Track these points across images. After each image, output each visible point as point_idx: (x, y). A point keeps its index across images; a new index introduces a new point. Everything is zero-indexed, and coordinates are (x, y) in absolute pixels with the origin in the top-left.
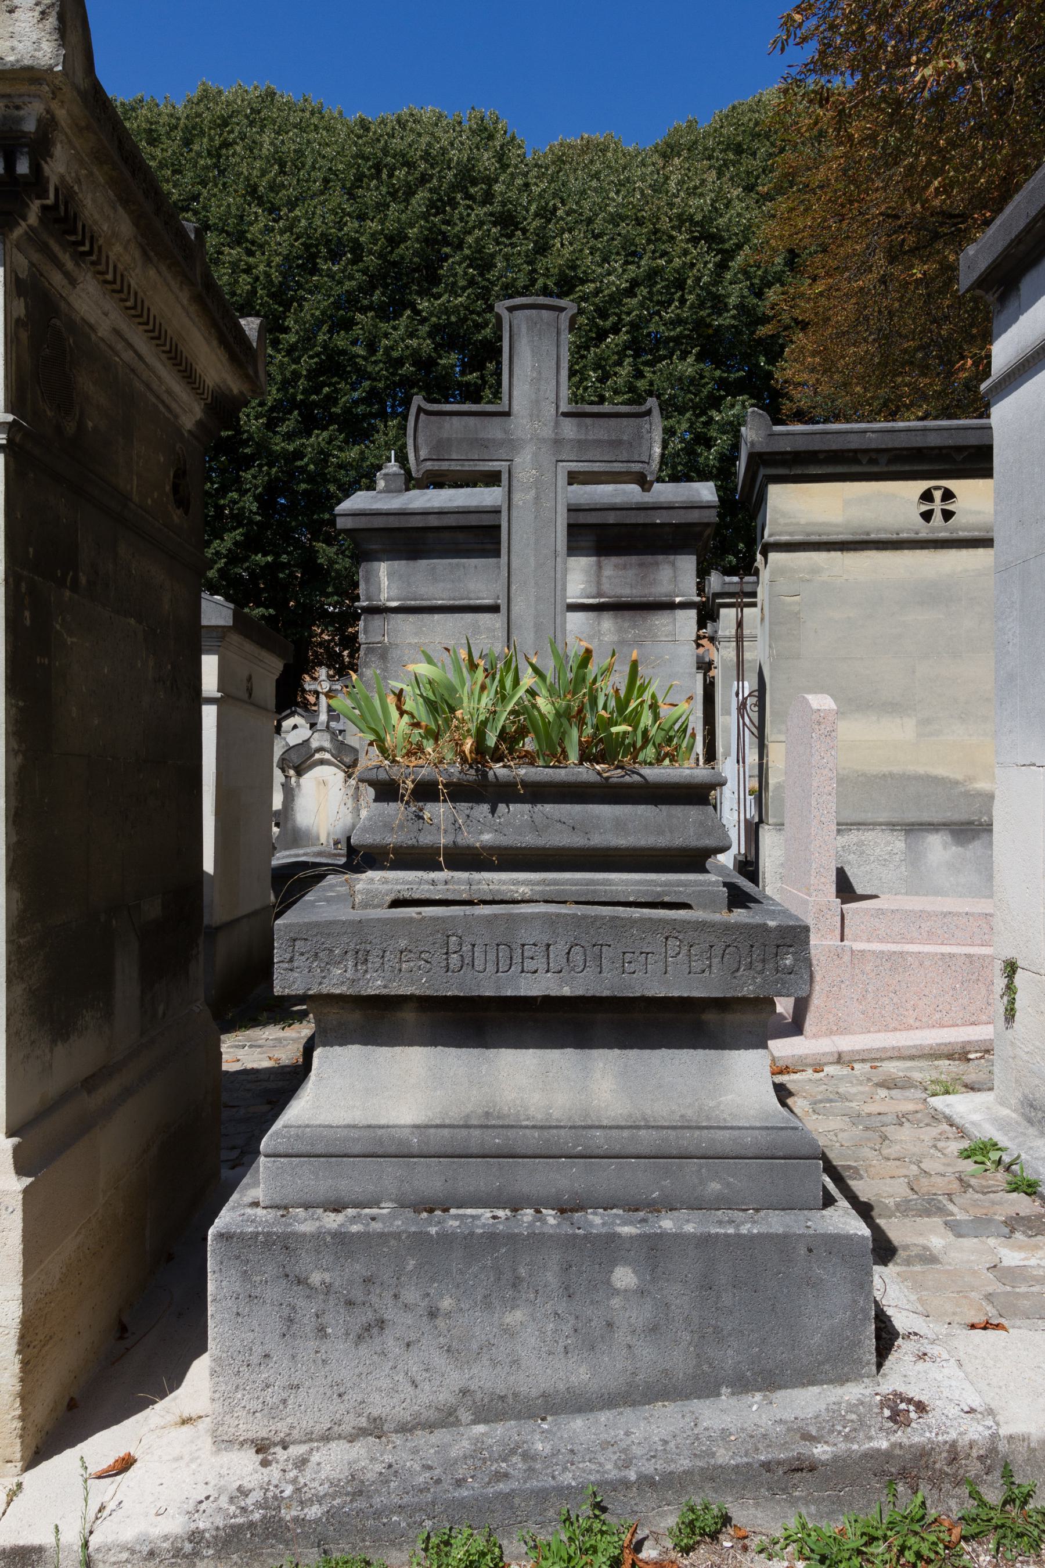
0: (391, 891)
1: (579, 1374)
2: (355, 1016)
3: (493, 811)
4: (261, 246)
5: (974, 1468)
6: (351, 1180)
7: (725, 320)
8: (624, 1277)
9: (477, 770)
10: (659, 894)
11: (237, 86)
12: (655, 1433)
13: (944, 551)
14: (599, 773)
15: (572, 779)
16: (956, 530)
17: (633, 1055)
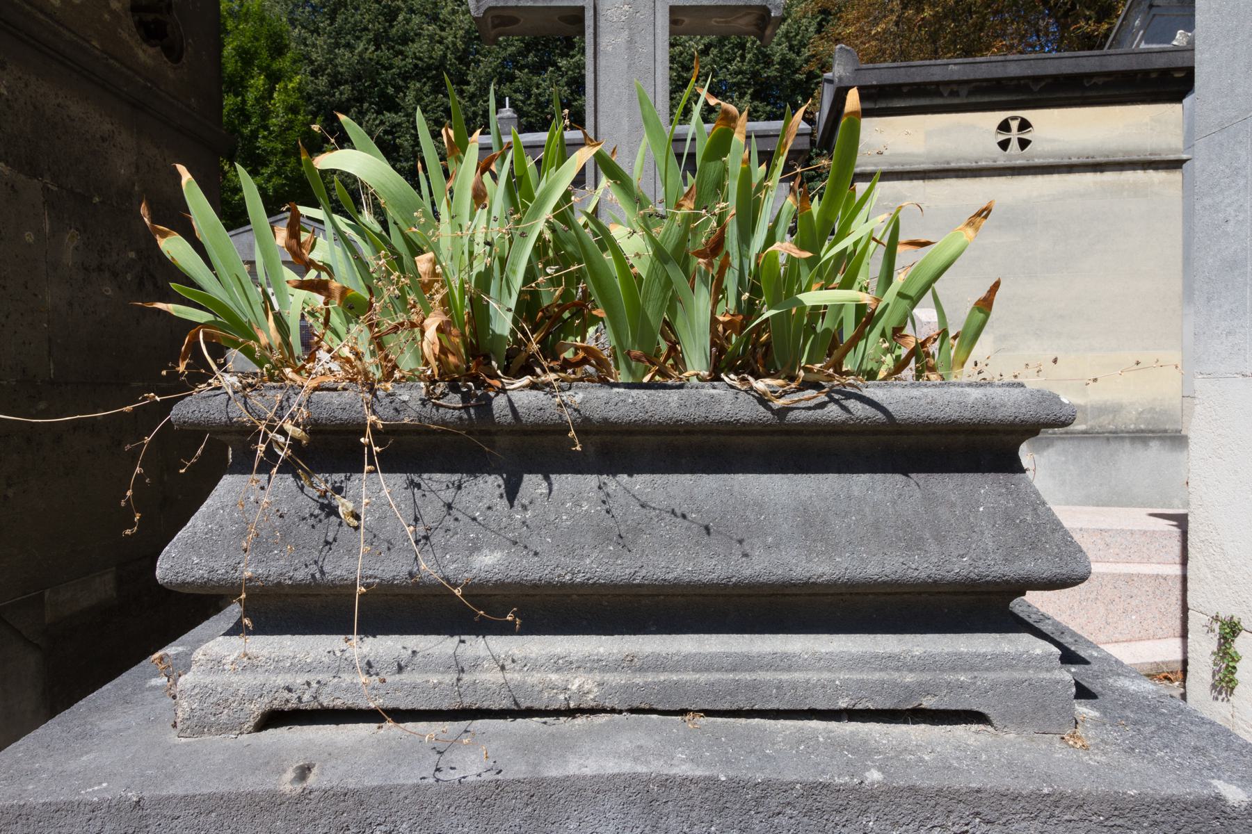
0: (260, 691)
3: (511, 492)
4: (449, 24)
7: (772, 72)
9: (466, 397)
10: (910, 691)
13: (1021, 178)
14: (762, 400)
15: (696, 414)
16: (1033, 158)
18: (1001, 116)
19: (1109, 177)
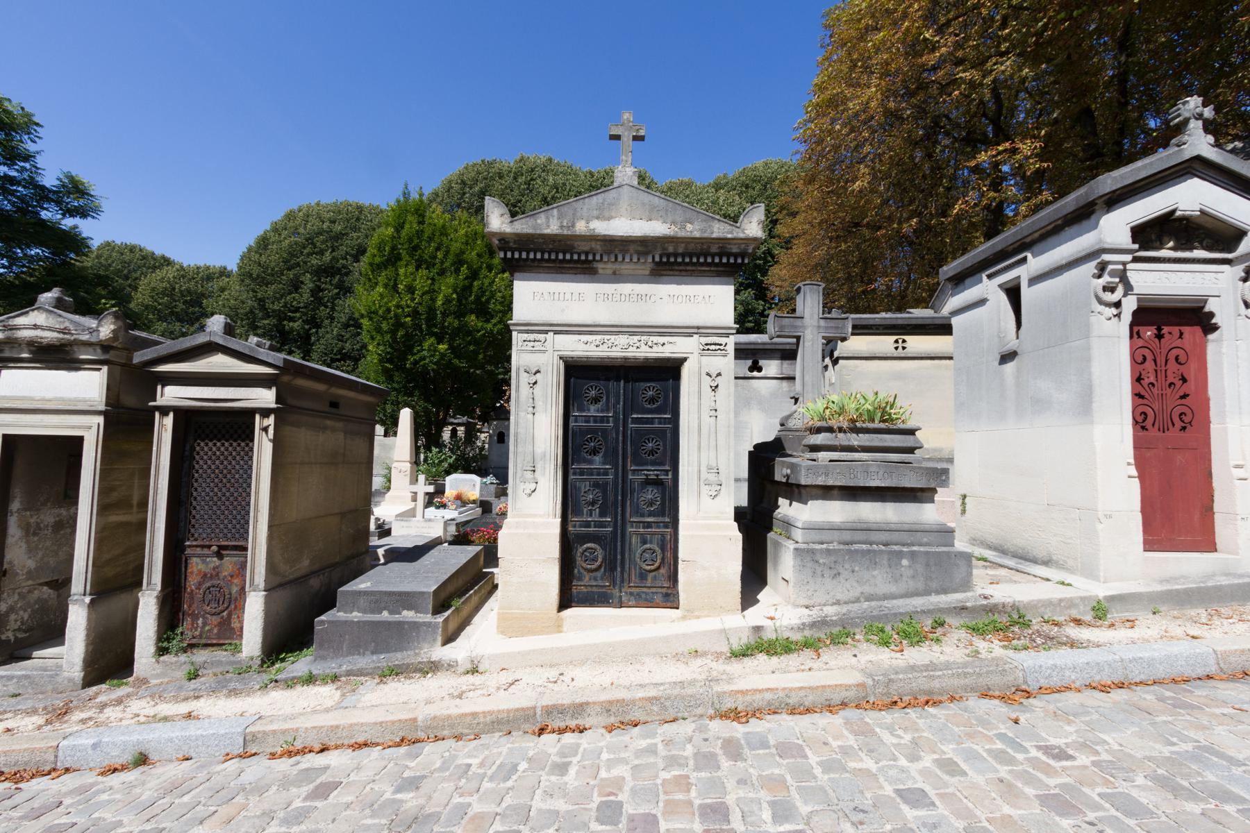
1: (893, 589)
2: (820, 492)
5: (1009, 609)
6: (826, 536)
8: (905, 562)
11: (537, 155)
12: (918, 603)
17: (897, 504)
18: (895, 337)
19: (936, 362)
